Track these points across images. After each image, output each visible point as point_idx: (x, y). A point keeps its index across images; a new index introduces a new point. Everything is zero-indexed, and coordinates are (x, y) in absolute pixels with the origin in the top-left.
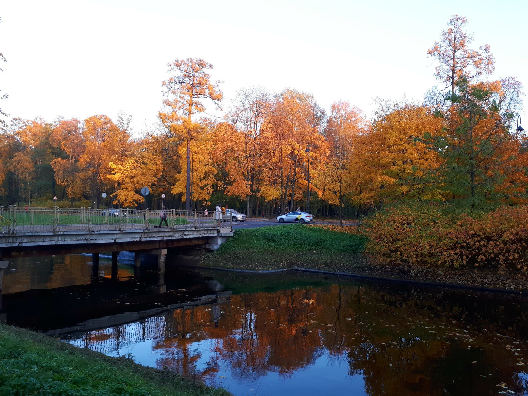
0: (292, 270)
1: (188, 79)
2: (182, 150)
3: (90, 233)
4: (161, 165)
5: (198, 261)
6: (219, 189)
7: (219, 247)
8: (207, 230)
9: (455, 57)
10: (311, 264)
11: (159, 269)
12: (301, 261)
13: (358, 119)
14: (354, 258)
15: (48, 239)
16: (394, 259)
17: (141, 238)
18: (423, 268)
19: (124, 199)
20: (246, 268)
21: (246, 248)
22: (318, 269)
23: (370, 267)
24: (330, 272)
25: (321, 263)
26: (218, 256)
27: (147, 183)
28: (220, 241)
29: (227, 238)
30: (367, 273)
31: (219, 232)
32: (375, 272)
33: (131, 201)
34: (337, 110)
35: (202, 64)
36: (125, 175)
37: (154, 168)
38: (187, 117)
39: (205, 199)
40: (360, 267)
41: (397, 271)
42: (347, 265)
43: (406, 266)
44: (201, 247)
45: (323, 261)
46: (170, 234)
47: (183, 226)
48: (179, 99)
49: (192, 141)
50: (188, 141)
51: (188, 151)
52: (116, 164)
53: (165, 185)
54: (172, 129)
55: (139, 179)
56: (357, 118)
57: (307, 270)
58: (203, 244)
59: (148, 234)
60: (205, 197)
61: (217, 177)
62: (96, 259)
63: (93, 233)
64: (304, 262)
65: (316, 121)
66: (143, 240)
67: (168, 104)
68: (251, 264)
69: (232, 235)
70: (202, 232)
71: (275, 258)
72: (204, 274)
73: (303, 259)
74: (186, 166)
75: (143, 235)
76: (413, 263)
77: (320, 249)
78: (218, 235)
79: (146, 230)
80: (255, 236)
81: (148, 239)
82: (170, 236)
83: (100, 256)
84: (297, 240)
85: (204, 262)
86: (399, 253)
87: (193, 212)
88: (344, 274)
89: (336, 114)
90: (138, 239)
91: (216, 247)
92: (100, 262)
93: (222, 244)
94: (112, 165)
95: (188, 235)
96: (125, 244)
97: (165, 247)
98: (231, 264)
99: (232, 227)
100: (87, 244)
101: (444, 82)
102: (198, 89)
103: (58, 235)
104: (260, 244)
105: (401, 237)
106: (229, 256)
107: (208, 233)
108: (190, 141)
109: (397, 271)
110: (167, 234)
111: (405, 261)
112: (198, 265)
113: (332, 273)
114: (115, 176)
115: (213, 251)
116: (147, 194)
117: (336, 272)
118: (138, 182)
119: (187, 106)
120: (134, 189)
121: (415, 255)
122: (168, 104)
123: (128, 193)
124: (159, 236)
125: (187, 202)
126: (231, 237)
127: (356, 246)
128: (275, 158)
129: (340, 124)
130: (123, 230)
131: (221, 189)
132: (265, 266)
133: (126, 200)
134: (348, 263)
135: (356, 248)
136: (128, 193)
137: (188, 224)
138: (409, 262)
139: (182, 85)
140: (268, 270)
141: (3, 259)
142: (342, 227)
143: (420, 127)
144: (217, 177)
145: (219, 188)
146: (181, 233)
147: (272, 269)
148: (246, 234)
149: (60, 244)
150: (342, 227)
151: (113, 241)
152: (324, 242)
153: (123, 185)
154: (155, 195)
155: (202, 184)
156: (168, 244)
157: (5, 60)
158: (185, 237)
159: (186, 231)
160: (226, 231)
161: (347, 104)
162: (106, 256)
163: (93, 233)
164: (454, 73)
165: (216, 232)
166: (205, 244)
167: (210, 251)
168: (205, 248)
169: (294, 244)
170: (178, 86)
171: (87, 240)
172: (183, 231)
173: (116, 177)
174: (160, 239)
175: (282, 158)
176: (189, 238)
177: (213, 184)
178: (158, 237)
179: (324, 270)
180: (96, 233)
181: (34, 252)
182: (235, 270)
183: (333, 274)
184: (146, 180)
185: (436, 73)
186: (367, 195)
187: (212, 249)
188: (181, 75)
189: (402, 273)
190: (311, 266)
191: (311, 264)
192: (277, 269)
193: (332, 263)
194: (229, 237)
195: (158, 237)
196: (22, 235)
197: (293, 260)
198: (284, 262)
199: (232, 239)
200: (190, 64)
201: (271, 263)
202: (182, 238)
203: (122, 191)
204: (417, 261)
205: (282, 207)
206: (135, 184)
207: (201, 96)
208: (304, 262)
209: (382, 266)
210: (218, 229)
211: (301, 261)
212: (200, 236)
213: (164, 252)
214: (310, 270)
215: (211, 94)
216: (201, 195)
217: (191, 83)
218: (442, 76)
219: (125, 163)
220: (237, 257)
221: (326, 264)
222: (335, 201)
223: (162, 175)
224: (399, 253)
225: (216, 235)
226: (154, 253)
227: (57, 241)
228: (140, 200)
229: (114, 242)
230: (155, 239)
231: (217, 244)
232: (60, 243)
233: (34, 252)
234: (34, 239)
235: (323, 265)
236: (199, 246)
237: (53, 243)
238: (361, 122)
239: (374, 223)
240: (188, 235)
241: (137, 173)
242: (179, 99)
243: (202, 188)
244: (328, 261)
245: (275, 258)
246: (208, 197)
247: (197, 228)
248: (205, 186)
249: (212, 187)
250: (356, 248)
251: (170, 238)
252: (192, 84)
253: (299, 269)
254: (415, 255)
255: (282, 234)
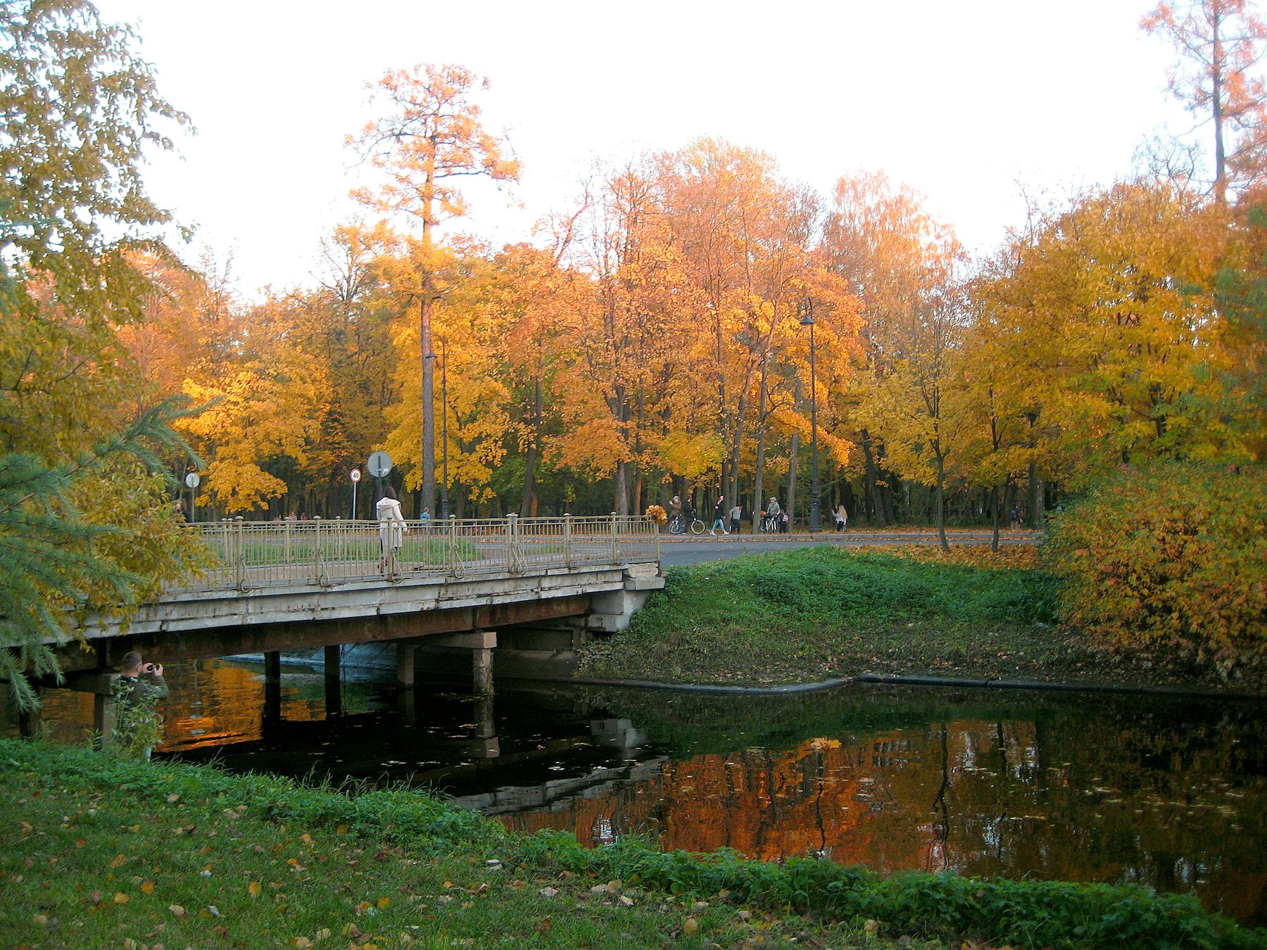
0: (860, 680)
1: (417, 124)
2: (404, 335)
3: (323, 590)
4: (327, 380)
5: (573, 665)
6: (521, 448)
7: (628, 622)
8: (597, 573)
9: (1220, 37)
10: (911, 661)
11: (480, 688)
12: (879, 653)
13: (917, 221)
14: (1032, 636)
15: (224, 609)
16: (1161, 633)
17: (437, 601)
18: (1249, 653)
19: (230, 489)
20: (700, 682)
21: (711, 621)
22: (938, 675)
23: (1089, 661)
24: (977, 681)
25: (941, 658)
26: (632, 650)
27: (293, 438)
28: (629, 605)
29: (649, 595)
30: (1084, 677)
31: (626, 577)
32: (1108, 674)
33: (249, 495)
34: (851, 194)
35: (463, 80)
36: (229, 415)
37: (311, 391)
38: (418, 235)
39: (475, 480)
40: (1060, 661)
41: (1170, 667)
42: (1021, 658)
43: (1200, 652)
44: (573, 625)
45: (947, 650)
46: (507, 587)
47: (488, 563)
48: (394, 183)
49: (436, 305)
50: (423, 303)
51: (423, 337)
52: (202, 383)
53: (339, 443)
54: (369, 277)
55: (269, 425)
56: (914, 217)
57: (905, 678)
58: (579, 616)
59: (454, 588)
60: (477, 475)
61: (513, 412)
62: (273, 668)
63: (329, 590)
64: (890, 656)
65: (796, 228)
66: (445, 605)
67: (361, 197)
68: (740, 669)
69: (661, 584)
70: (584, 580)
71: (802, 649)
72: (589, 698)
73: (883, 646)
74: (418, 382)
75: (443, 591)
76: (1218, 642)
77: (924, 615)
78: (624, 586)
79: (453, 579)
80: (730, 585)
81: (456, 604)
82: (506, 594)
83: (283, 659)
84: (852, 593)
85: (592, 668)
86: (1175, 615)
87: (563, 521)
88: (1019, 683)
89: (847, 207)
90: (432, 605)
91: (620, 623)
92: (282, 675)
93: (635, 613)
94: (192, 389)
95: (550, 589)
96: (390, 620)
97: (488, 626)
98: (678, 670)
99: (659, 563)
100: (314, 623)
101: (1186, 108)
102: (445, 148)
103: (247, 599)
104: (751, 610)
105: (1173, 568)
106: (666, 647)
107: (599, 582)
108: (429, 306)
109: (1170, 667)
110: (499, 588)
111: (1196, 637)
112: (576, 676)
113: (983, 682)
114: (201, 420)
115: (610, 634)
116: (386, 470)
117: (992, 679)
118: (267, 435)
119: (418, 204)
120: (256, 459)
121: (1224, 617)
122: (361, 197)
123: (240, 470)
124: (482, 593)
125: (426, 491)
126: (659, 590)
127: (1025, 602)
128: (699, 346)
129: (865, 235)
130: (247, 589)
131: (529, 447)
132: (781, 672)
133: (234, 493)
134: (1022, 653)
135: (1028, 609)
136: (240, 470)
137: (484, 558)
138: (1208, 639)
139: (399, 140)
140: (794, 684)
141: (116, 668)
142: (946, 548)
143: (1172, 251)
144: (513, 412)
145: (524, 444)
146: (532, 584)
147: (804, 681)
148: (702, 581)
149: (253, 622)
150: (946, 548)
151: (373, 612)
152: (929, 595)
153: (223, 448)
154: (310, 473)
155: (469, 434)
156: (493, 615)
157: (346, 174)
158: (544, 595)
159: (546, 576)
160: (644, 575)
161: (879, 179)
162: (292, 660)
163: (329, 590)
164: (1217, 83)
165: (618, 577)
166: (586, 615)
167: (601, 635)
168: (586, 627)
169: (846, 605)
170: (390, 144)
171: (313, 610)
172: (538, 577)
173: (205, 424)
174: (483, 602)
175: (721, 347)
176: (553, 599)
177: (506, 433)
178: (479, 596)
179: (956, 676)
180: (336, 589)
181: (183, 647)
182: (698, 687)
183: (985, 685)
184: (289, 431)
185: (1166, 85)
186: (1029, 452)
187: (607, 630)
188: (400, 111)
189: (1187, 672)
190: (912, 667)
191: (910, 661)
192: (820, 681)
193: (974, 655)
194: (652, 591)
195: (479, 596)
196: (170, 600)
197: (856, 653)
198: (829, 659)
199: (662, 598)
200: (426, 80)
201: (793, 663)
202: (535, 597)
203: (223, 465)
204: (1229, 635)
205: (728, 496)
206: (257, 444)
207: (457, 170)
208: (890, 656)
209: (1128, 656)
210: (623, 570)
211: (879, 653)
212: (580, 593)
213: (490, 639)
214: (914, 677)
215: (490, 165)
216: (464, 470)
217: (429, 134)
218: (1181, 91)
219: (227, 380)
220: (693, 651)
221: (957, 658)
222: (920, 473)
223: (330, 413)
224: (1175, 615)
225: (619, 586)
226: (459, 642)
227: (244, 617)
228: (274, 492)
229: (375, 614)
230: (473, 603)
231: (622, 613)
232: (253, 620)
233: (183, 647)
234: (192, 611)
235: (947, 660)
236: (566, 619)
237: (236, 621)
238: (926, 227)
239: (1091, 534)
240: (550, 589)
241: (265, 410)
242: (394, 183)
243: (469, 448)
244: (963, 651)
245: (802, 649)
246: (484, 475)
247: (575, 568)
248: (479, 440)
249: (500, 443)
250: (1028, 609)
251: (507, 600)
252: (433, 138)
253: (880, 676)
254: (1224, 617)
255: (803, 579)
